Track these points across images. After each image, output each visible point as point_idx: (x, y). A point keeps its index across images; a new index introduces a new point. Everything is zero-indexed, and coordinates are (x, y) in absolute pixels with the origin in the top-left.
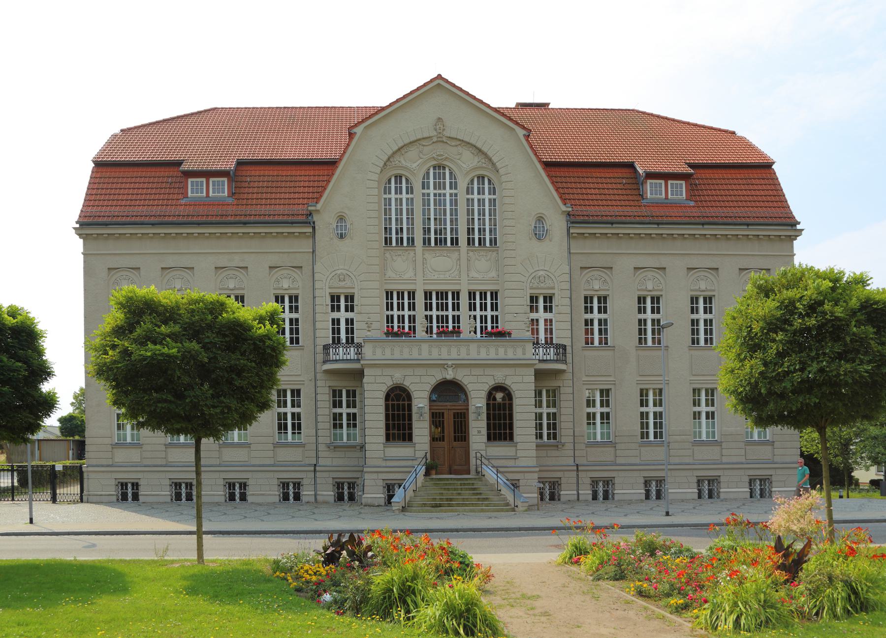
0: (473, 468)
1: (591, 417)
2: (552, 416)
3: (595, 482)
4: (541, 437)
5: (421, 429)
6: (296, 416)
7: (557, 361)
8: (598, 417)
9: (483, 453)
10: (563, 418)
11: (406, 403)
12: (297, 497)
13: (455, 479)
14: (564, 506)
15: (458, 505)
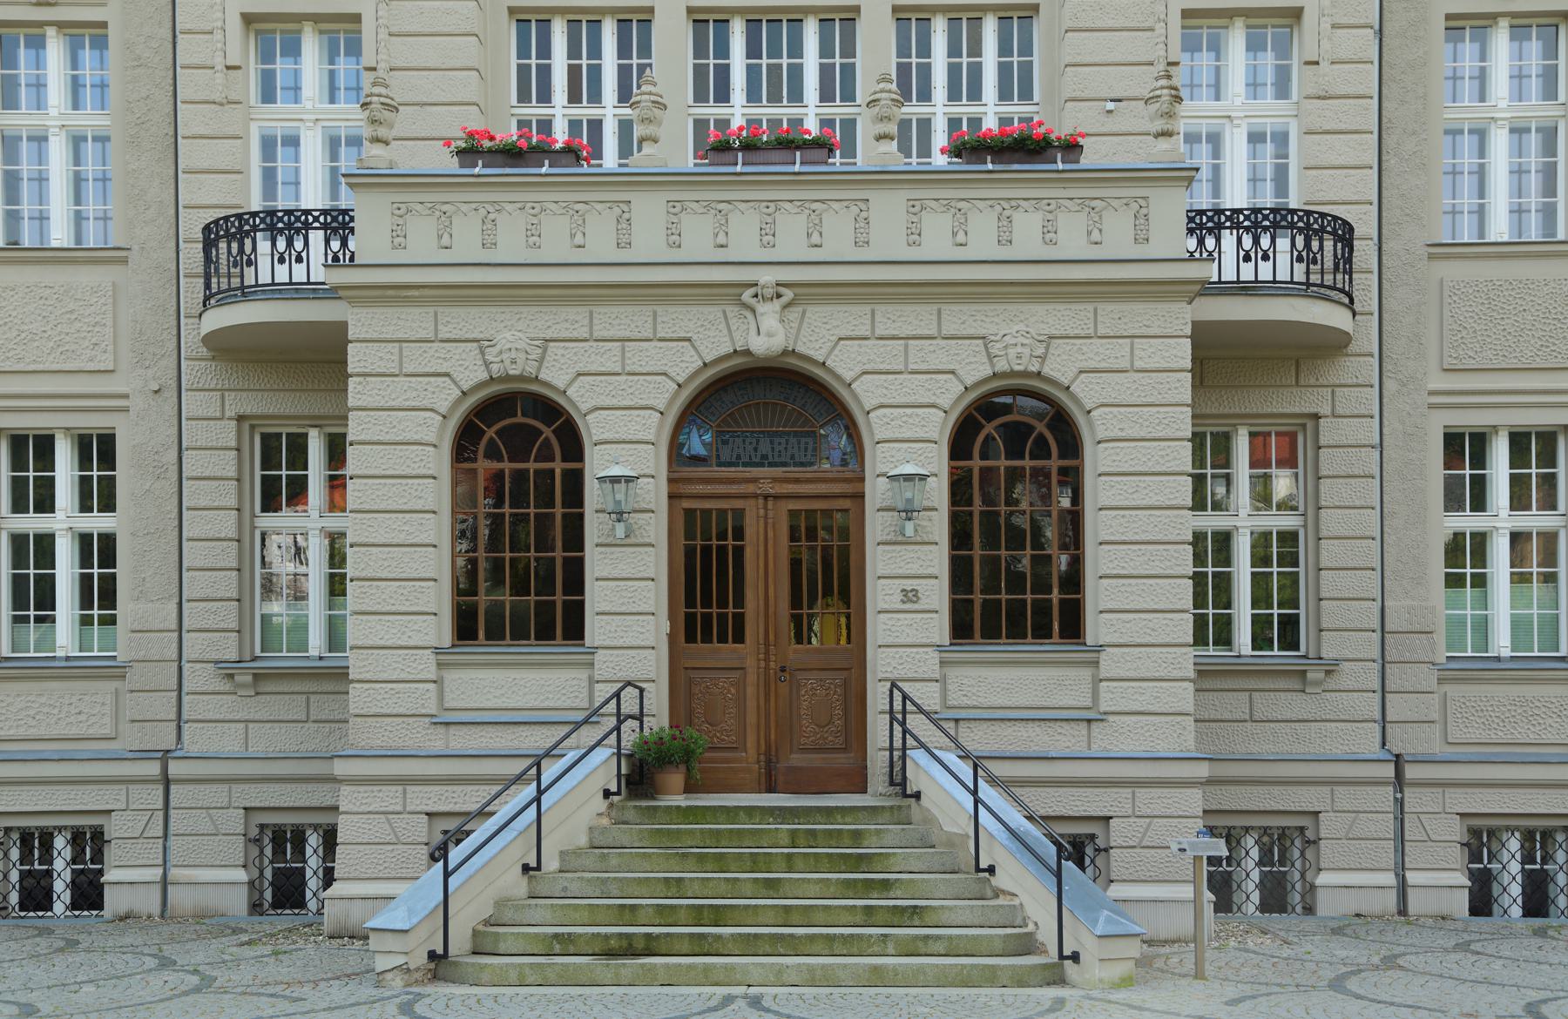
0: (877, 762)
1: (1466, 554)
2: (1278, 551)
3: (1480, 841)
4: (1224, 637)
5: (629, 587)
6: (99, 551)
7: (1306, 289)
8: (1500, 550)
9: (926, 695)
10: (1331, 553)
11: (558, 467)
12: (88, 894)
13: (770, 811)
14: (1345, 951)
15: (750, 946)
